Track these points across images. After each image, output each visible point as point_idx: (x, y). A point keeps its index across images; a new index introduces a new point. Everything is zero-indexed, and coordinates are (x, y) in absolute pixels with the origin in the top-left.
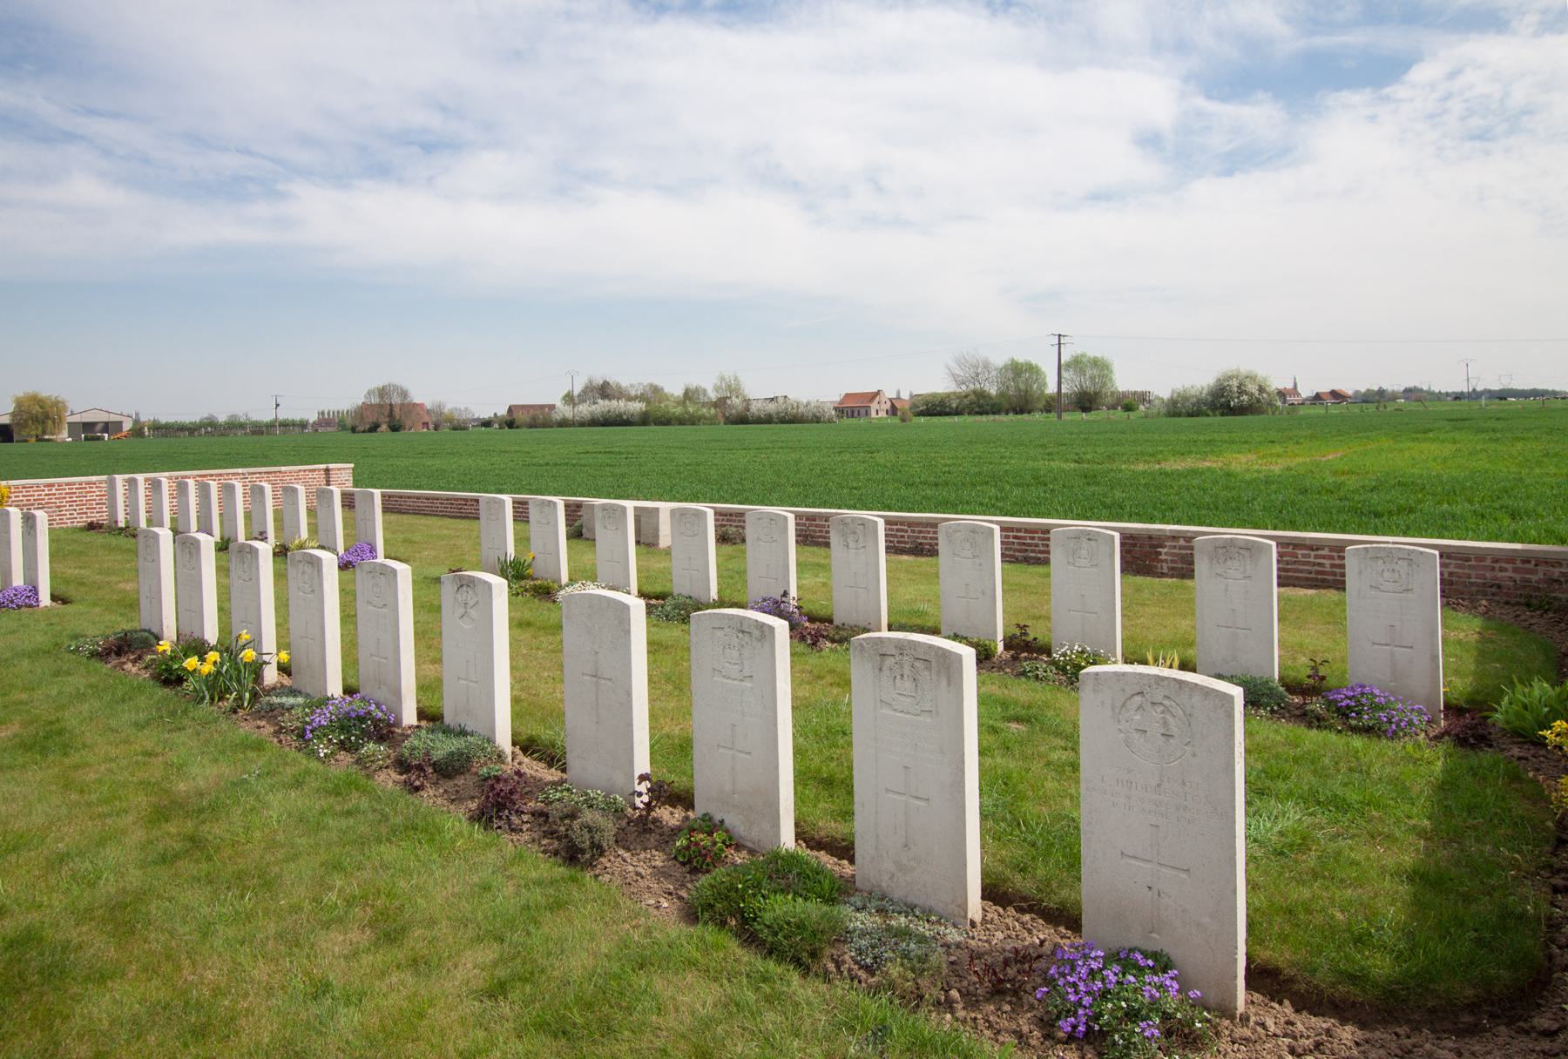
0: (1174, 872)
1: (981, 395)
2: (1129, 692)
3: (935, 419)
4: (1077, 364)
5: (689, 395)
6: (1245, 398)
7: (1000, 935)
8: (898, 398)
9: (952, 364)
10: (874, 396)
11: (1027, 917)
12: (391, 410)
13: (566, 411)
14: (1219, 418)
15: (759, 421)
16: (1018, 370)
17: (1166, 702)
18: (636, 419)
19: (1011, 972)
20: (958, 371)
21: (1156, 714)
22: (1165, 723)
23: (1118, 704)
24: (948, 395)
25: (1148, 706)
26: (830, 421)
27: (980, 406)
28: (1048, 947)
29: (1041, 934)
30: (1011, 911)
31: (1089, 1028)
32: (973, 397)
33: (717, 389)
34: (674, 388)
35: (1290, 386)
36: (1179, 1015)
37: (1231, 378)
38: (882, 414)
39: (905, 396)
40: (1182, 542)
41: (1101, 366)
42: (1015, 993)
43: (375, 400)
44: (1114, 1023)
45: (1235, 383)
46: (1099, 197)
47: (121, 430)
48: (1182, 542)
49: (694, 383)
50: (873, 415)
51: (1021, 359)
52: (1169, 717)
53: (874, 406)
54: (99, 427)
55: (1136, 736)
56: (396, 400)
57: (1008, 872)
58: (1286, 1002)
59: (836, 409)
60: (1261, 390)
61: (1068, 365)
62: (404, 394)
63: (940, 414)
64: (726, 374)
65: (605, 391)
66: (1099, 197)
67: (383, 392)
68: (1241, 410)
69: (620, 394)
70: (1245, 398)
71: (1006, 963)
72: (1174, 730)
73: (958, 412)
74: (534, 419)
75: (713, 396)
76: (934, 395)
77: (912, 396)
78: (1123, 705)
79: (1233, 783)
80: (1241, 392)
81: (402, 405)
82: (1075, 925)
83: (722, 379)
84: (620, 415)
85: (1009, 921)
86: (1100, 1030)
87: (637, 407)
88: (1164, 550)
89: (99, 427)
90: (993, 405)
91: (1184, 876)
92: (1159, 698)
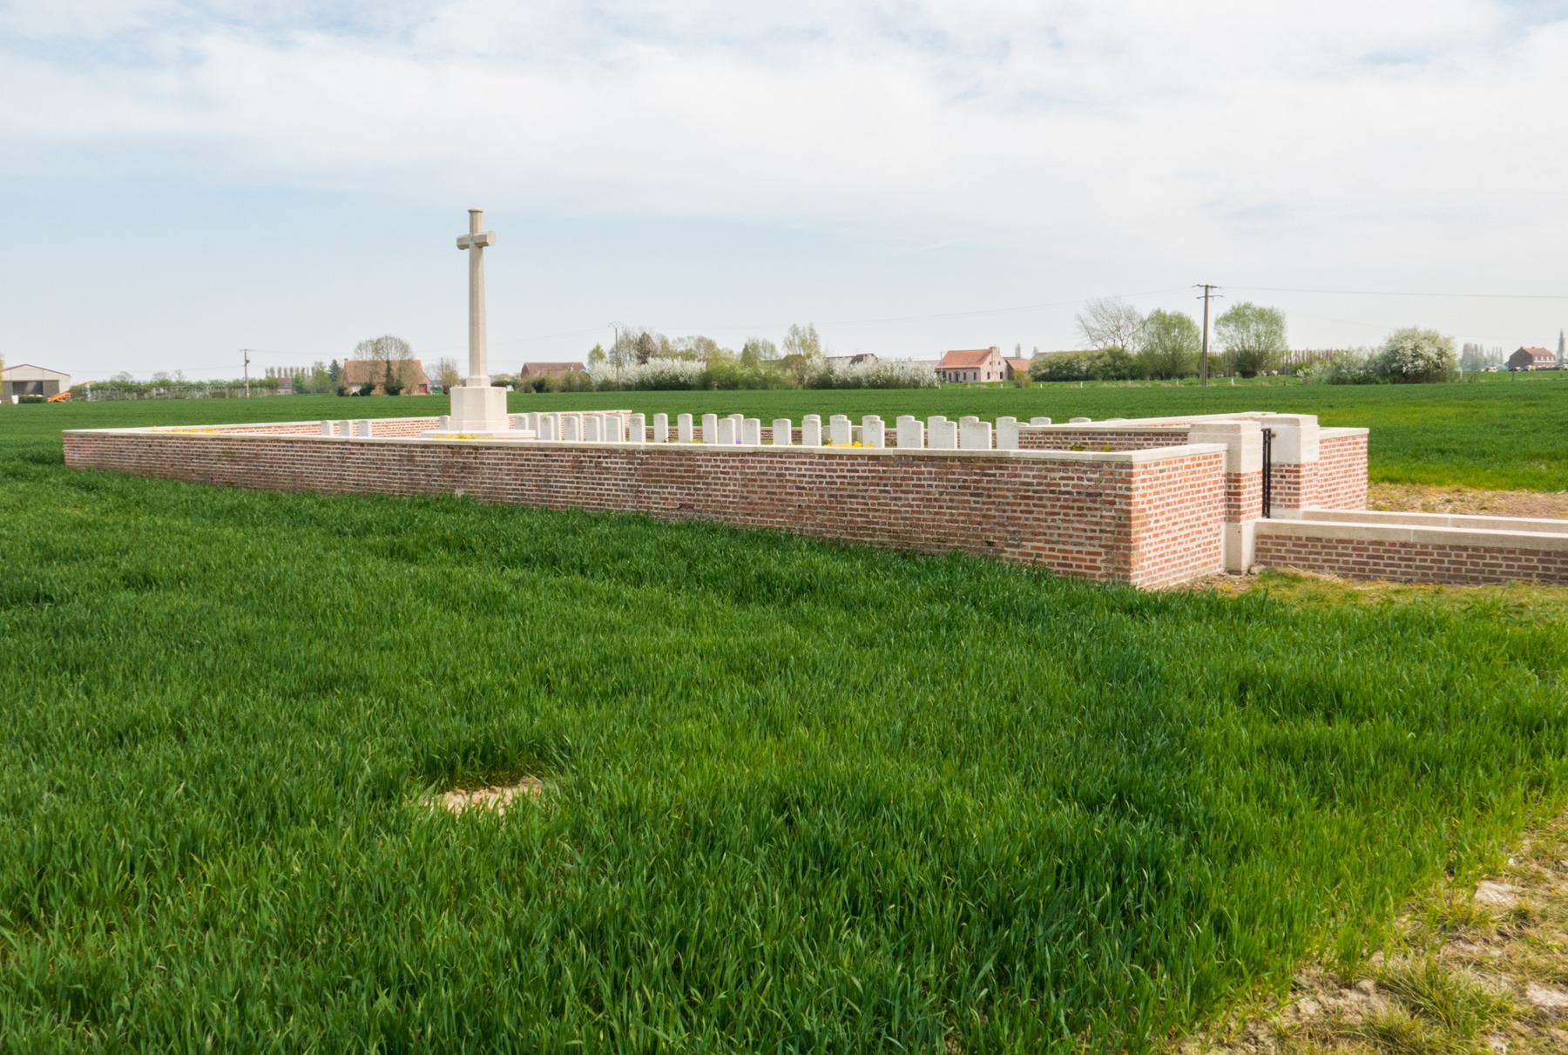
1: (1117, 355)
3: (1057, 385)
5: (749, 355)
6: (1420, 363)
8: (1018, 358)
9: (1086, 315)
10: (983, 355)
12: (389, 369)
13: (604, 371)
14: (1389, 385)
15: (845, 385)
16: (1167, 324)
18: (694, 381)
20: (1093, 324)
24: (1077, 355)
26: (931, 386)
27: (1116, 370)
32: (1108, 359)
33: (790, 344)
34: (731, 345)
38: (995, 378)
39: (1027, 355)
41: (1270, 319)
43: (368, 356)
45: (1409, 345)
46: (1388, 59)
47: (57, 391)
49: (760, 336)
50: (984, 379)
51: (1169, 310)
53: (985, 368)
54: (30, 387)
56: (394, 356)
59: (938, 371)
62: (404, 348)
63: (1066, 379)
64: (800, 327)
65: (643, 350)
66: (1388, 59)
67: (377, 346)
69: (667, 352)
70: (1420, 363)
73: (1087, 377)
74: (568, 380)
75: (782, 353)
76: (1060, 355)
77: (1037, 354)
79: (219, 421)
80: (1416, 356)
81: (402, 362)
83: (795, 331)
84: (676, 378)
87: (695, 367)
89: (30, 387)
90: (1132, 369)
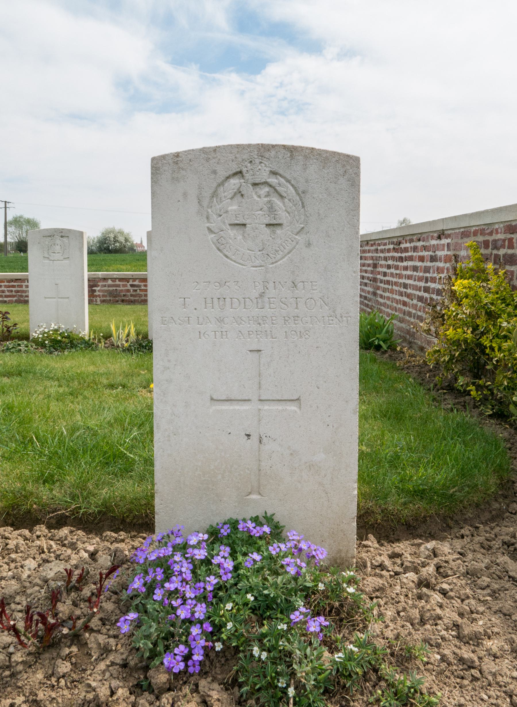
0: (280, 407)
2: (222, 173)
4: (17, 222)
6: (118, 244)
7: (31, 564)
11: (65, 531)
17: (273, 180)
19: (64, 608)
21: (258, 198)
22: (271, 209)
23: (207, 193)
25: (248, 190)
28: (105, 560)
29: (86, 548)
30: (41, 529)
31: (208, 651)
35: (139, 242)
36: (321, 587)
37: (110, 232)
40: (110, 282)
42: (75, 638)
44: (242, 630)
45: (112, 236)
48: (110, 282)
52: (276, 201)
55: (232, 232)
57: (30, 487)
58: (371, 536)
60: (126, 240)
61: (11, 223)
68: (116, 251)
70: (118, 244)
71: (55, 597)
72: (283, 217)
78: (214, 194)
80: (116, 241)
82: (139, 520)
85: (43, 543)
86: (227, 648)
88: (97, 289)
91: (292, 408)
92: (264, 175)
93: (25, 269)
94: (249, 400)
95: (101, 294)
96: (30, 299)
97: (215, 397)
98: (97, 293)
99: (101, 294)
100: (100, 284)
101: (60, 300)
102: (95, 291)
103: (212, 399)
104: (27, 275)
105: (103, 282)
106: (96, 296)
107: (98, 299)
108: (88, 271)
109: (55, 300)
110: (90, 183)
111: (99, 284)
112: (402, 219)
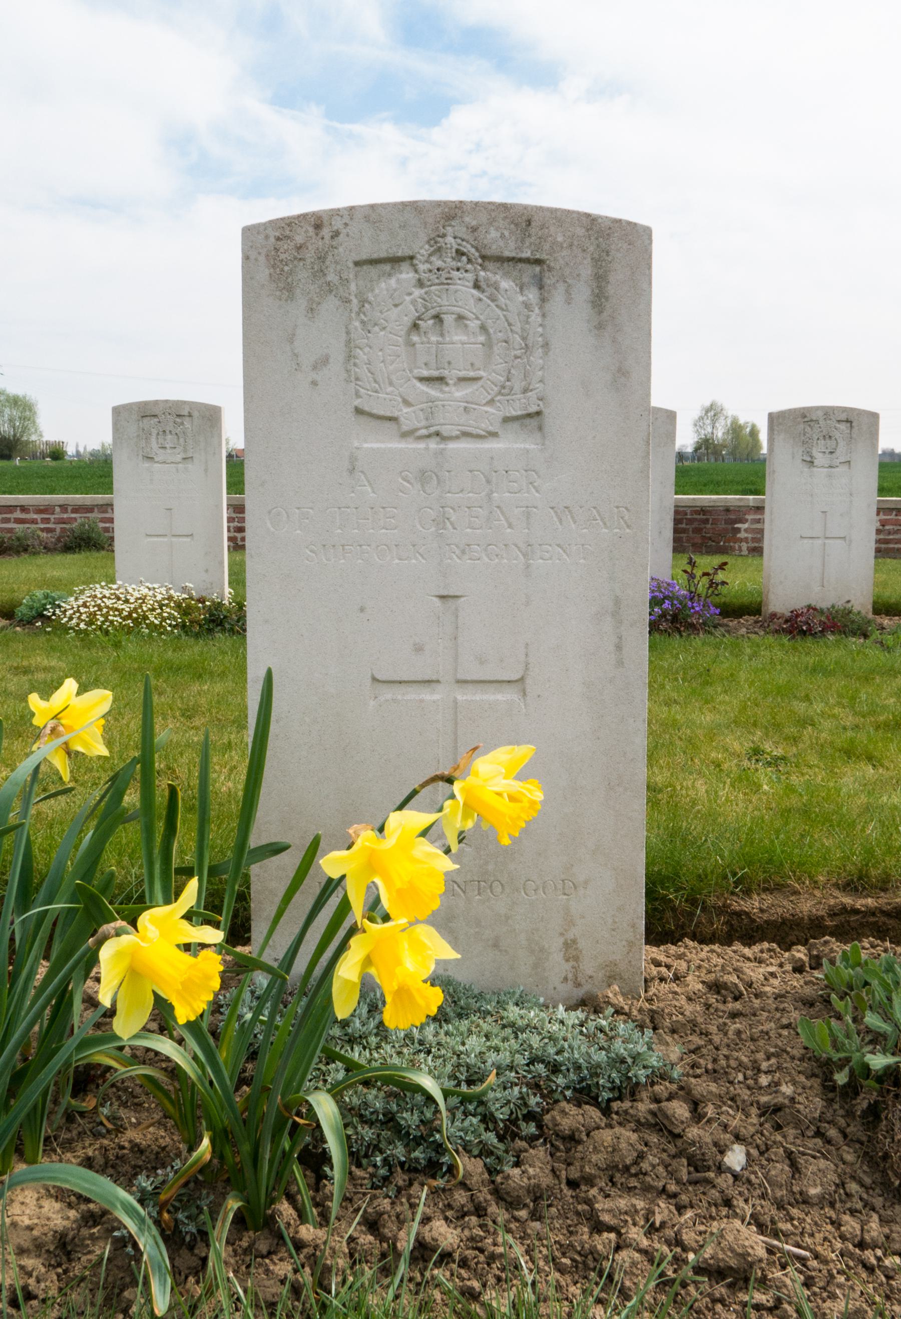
93: (108, 488)
94: (438, 681)
95: (750, 536)
96: (247, 544)
97: (379, 677)
98: (742, 535)
99: (750, 536)
100: (749, 517)
101: (174, 539)
102: (739, 530)
103: (375, 679)
104: (763, 501)
105: (755, 513)
106: (741, 540)
107: (744, 546)
108: (228, 493)
109: (166, 539)
110: (114, 323)
111: (747, 517)
112: (707, 404)
